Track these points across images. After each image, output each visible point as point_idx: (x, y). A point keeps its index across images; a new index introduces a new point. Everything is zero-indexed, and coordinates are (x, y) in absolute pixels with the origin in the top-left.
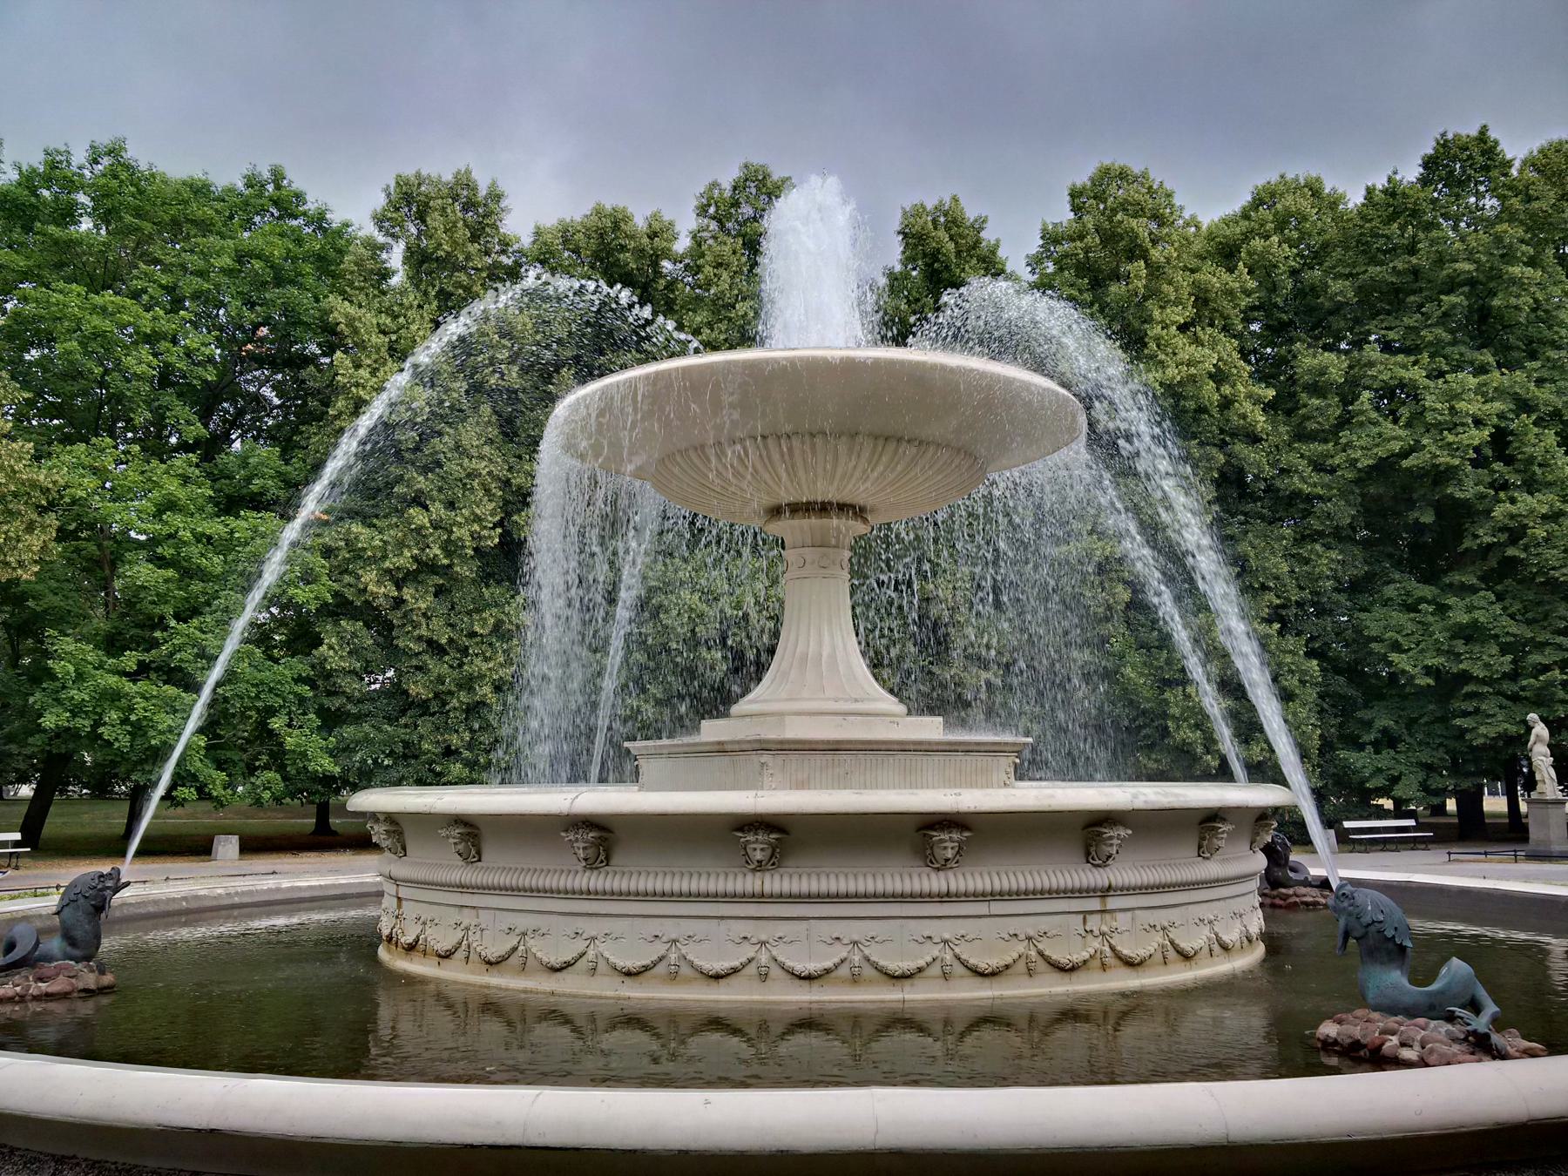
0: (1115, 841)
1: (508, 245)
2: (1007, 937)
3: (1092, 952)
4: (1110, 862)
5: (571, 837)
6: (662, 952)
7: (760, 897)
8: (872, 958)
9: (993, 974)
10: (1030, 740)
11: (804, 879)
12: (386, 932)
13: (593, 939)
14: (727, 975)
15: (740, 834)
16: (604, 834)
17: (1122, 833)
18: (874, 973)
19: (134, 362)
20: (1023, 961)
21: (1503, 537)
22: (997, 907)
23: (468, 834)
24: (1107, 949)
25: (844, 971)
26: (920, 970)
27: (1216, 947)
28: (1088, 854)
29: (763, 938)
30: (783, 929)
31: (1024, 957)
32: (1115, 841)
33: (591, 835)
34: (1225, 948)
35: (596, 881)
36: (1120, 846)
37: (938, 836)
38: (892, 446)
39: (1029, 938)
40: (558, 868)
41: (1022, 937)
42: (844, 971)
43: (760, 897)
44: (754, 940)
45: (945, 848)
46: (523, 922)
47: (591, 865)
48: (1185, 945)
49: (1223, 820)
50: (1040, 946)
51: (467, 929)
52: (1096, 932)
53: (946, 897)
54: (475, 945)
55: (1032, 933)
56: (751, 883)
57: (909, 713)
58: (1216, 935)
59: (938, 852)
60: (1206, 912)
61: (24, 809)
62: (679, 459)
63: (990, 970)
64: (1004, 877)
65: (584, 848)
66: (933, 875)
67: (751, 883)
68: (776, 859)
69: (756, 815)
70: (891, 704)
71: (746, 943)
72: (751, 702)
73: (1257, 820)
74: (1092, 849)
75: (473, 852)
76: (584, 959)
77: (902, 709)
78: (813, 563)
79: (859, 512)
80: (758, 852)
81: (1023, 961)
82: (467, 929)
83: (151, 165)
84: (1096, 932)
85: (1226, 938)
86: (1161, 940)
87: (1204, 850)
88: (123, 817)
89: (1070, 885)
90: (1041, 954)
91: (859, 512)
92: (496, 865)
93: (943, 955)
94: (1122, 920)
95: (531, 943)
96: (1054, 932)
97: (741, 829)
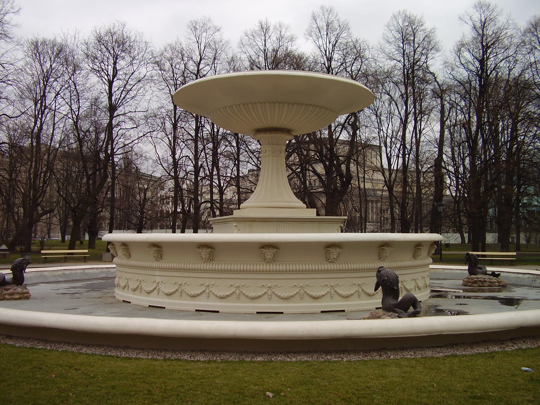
0: (389, 252)
1: (274, 50)
2: (352, 285)
3: (355, 291)
5: (201, 251)
6: (266, 291)
9: (347, 297)
10: (346, 217)
12: (116, 283)
13: (238, 287)
14: (257, 298)
15: (263, 250)
20: (357, 292)
21: (96, 61)
23: (158, 250)
26: (323, 296)
27: (417, 288)
29: (270, 285)
33: (208, 250)
36: (390, 253)
38: (311, 107)
41: (357, 285)
45: (334, 255)
46: (141, 278)
47: (157, 260)
50: (363, 288)
51: (141, 281)
52: (329, 286)
56: (267, 267)
57: (307, 208)
58: (417, 284)
59: (332, 256)
61: (88, 242)
62: (222, 110)
64: (375, 264)
65: (153, 253)
66: (329, 264)
68: (211, 259)
69: (269, 243)
70: (300, 204)
71: (263, 288)
72: (248, 202)
75: (160, 257)
77: (305, 206)
78: (269, 151)
79: (288, 131)
81: (357, 292)
82: (141, 281)
87: (415, 256)
88: (444, 254)
89: (389, 266)
90: (363, 290)
91: (288, 131)
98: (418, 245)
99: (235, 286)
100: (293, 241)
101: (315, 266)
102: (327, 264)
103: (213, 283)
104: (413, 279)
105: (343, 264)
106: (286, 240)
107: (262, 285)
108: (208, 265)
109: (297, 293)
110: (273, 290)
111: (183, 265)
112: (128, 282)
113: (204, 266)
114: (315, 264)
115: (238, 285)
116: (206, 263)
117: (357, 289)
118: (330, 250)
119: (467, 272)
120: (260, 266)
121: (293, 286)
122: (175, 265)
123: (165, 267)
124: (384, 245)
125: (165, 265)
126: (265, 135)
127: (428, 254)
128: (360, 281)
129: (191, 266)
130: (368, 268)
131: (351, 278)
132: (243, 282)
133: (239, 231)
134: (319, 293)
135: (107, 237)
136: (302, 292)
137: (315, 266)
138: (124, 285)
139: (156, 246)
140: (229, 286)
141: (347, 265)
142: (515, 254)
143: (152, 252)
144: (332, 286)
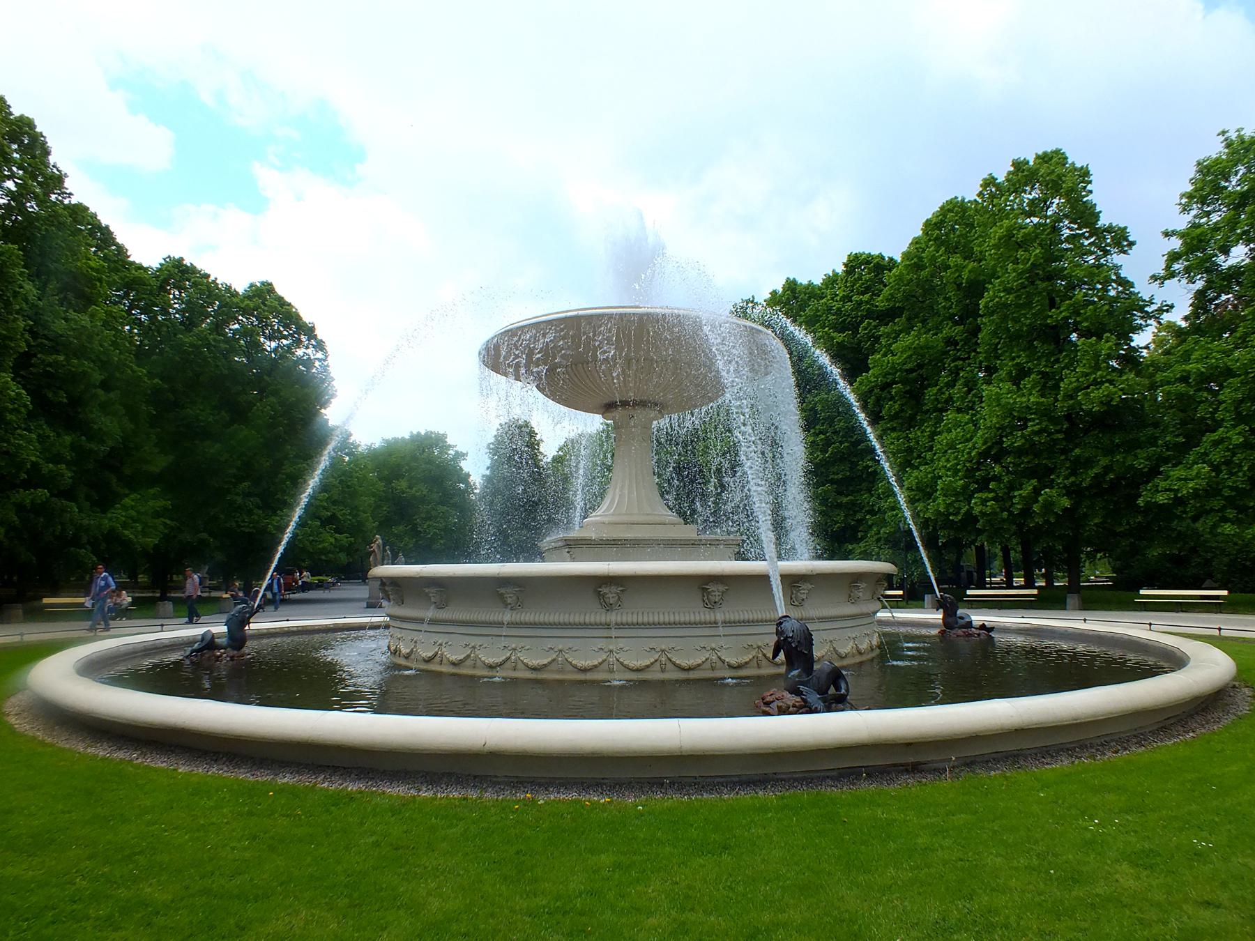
4: (803, 603)
6: (554, 656)
8: (673, 660)
11: (577, 615)
13: (514, 649)
17: (810, 587)
18: (524, 667)
19: (38, 253)
25: (605, 666)
29: (663, 647)
32: (717, 593)
34: (860, 653)
37: (711, 588)
39: (759, 647)
41: (755, 646)
42: (707, 665)
44: (607, 650)
48: (843, 651)
52: (708, 648)
53: (607, 626)
63: (687, 667)
64: (727, 614)
68: (518, 606)
76: (509, 662)
81: (755, 660)
82: (441, 645)
83: (1100, 212)
85: (860, 647)
93: (711, 656)
95: (478, 652)
96: (679, 648)
100: (516, 575)
101: (648, 617)
105: (741, 613)
106: (406, 575)
109: (656, 661)
110: (566, 656)
111: (488, 617)
112: (415, 646)
114: (733, 613)
115: (513, 646)
117: (707, 656)
119: (941, 621)
121: (648, 649)
126: (790, 375)
131: (677, 637)
132: (522, 642)
133: (573, 560)
134: (639, 663)
137: (648, 617)
138: (408, 651)
142: (901, 592)
144: (713, 649)
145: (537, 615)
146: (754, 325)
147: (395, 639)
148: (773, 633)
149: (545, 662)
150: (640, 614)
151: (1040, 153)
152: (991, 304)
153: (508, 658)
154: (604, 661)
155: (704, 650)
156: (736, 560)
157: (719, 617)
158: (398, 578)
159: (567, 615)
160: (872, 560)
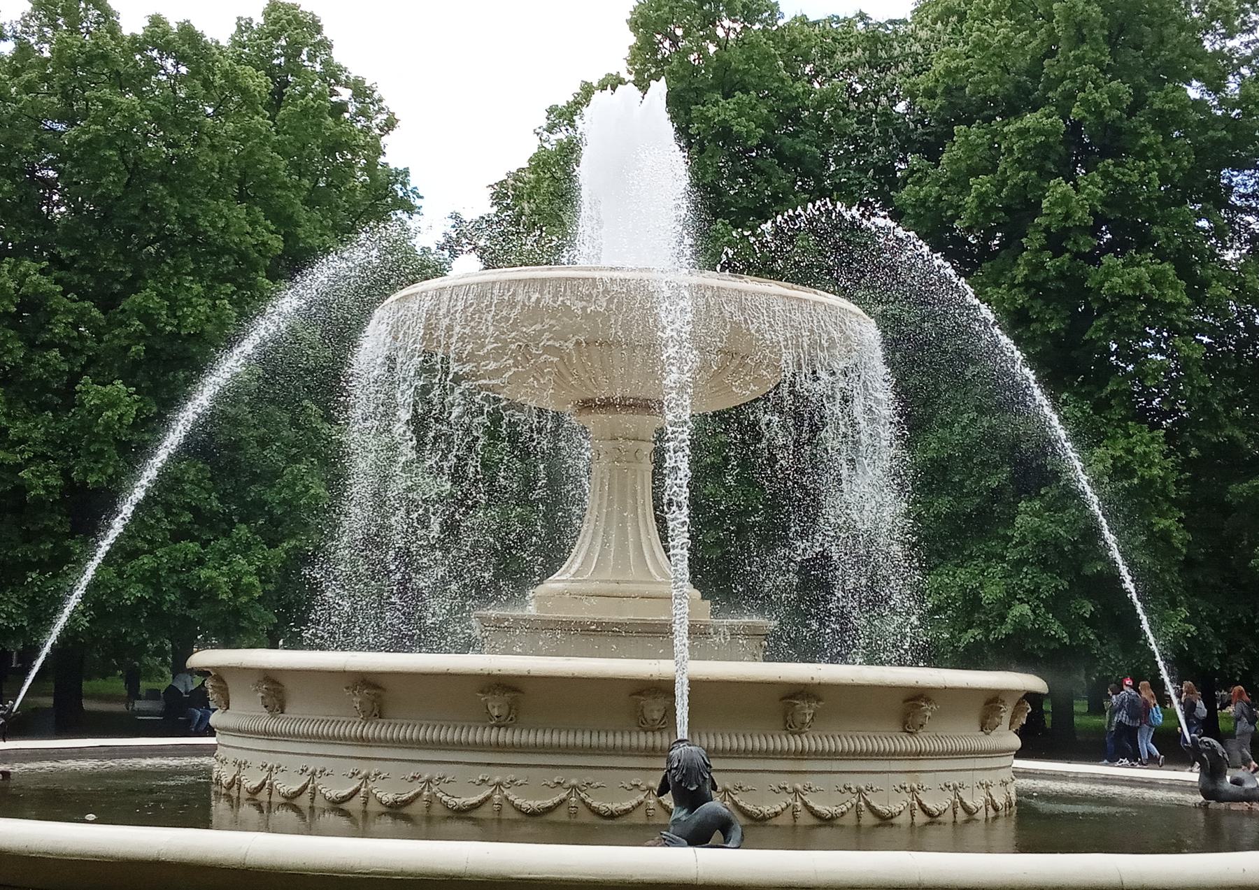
3: (784, 805)
7: (499, 747)
13: (499, 784)
14: (620, 815)
16: (378, 692)
22: (980, 763)
23: (274, 690)
24: (862, 803)
28: (905, 723)
30: (450, 771)
31: (791, 808)
35: (370, 731)
40: (342, 719)
41: (854, 790)
43: (499, 747)
44: (644, 787)
49: (928, 700)
51: (271, 770)
52: (790, 790)
54: (319, 787)
55: (728, 786)
56: (491, 735)
58: (990, 796)
60: (986, 777)
64: (719, 738)
66: (790, 737)
67: (491, 735)
68: (791, 726)
73: (987, 703)
74: (789, 718)
76: (488, 804)
80: (496, 709)
84: (854, 790)
86: (909, 800)
90: (805, 804)
92: (307, 717)
94: (925, 780)
96: (597, 784)
97: (640, 693)
98: (992, 701)
99: (566, 785)
102: (638, 733)
103: (376, 770)
104: (982, 785)
107: (633, 783)
108: (517, 732)
110: (583, 795)
113: (810, 744)
115: (497, 779)
116: (495, 729)
118: (795, 704)
120: (654, 738)
122: (370, 731)
123: (382, 735)
124: (916, 697)
125: (370, 731)
127: (1010, 725)
128: (854, 782)
129: (758, 743)
130: (728, 746)
132: (511, 774)
135: (203, 658)
136: (652, 801)
138: (229, 779)
139: (366, 681)
140: (477, 782)
141: (735, 739)
143: (260, 694)
145: (423, 730)
146: (493, 346)
147: (230, 765)
148: (715, 770)
149: (549, 803)
150: (458, 730)
151: (173, 20)
152: (273, 228)
153: (488, 799)
154: (640, 804)
155: (636, 790)
156: (764, 661)
157: (808, 742)
158: (520, 677)
159: (587, 735)
160: (814, 662)
